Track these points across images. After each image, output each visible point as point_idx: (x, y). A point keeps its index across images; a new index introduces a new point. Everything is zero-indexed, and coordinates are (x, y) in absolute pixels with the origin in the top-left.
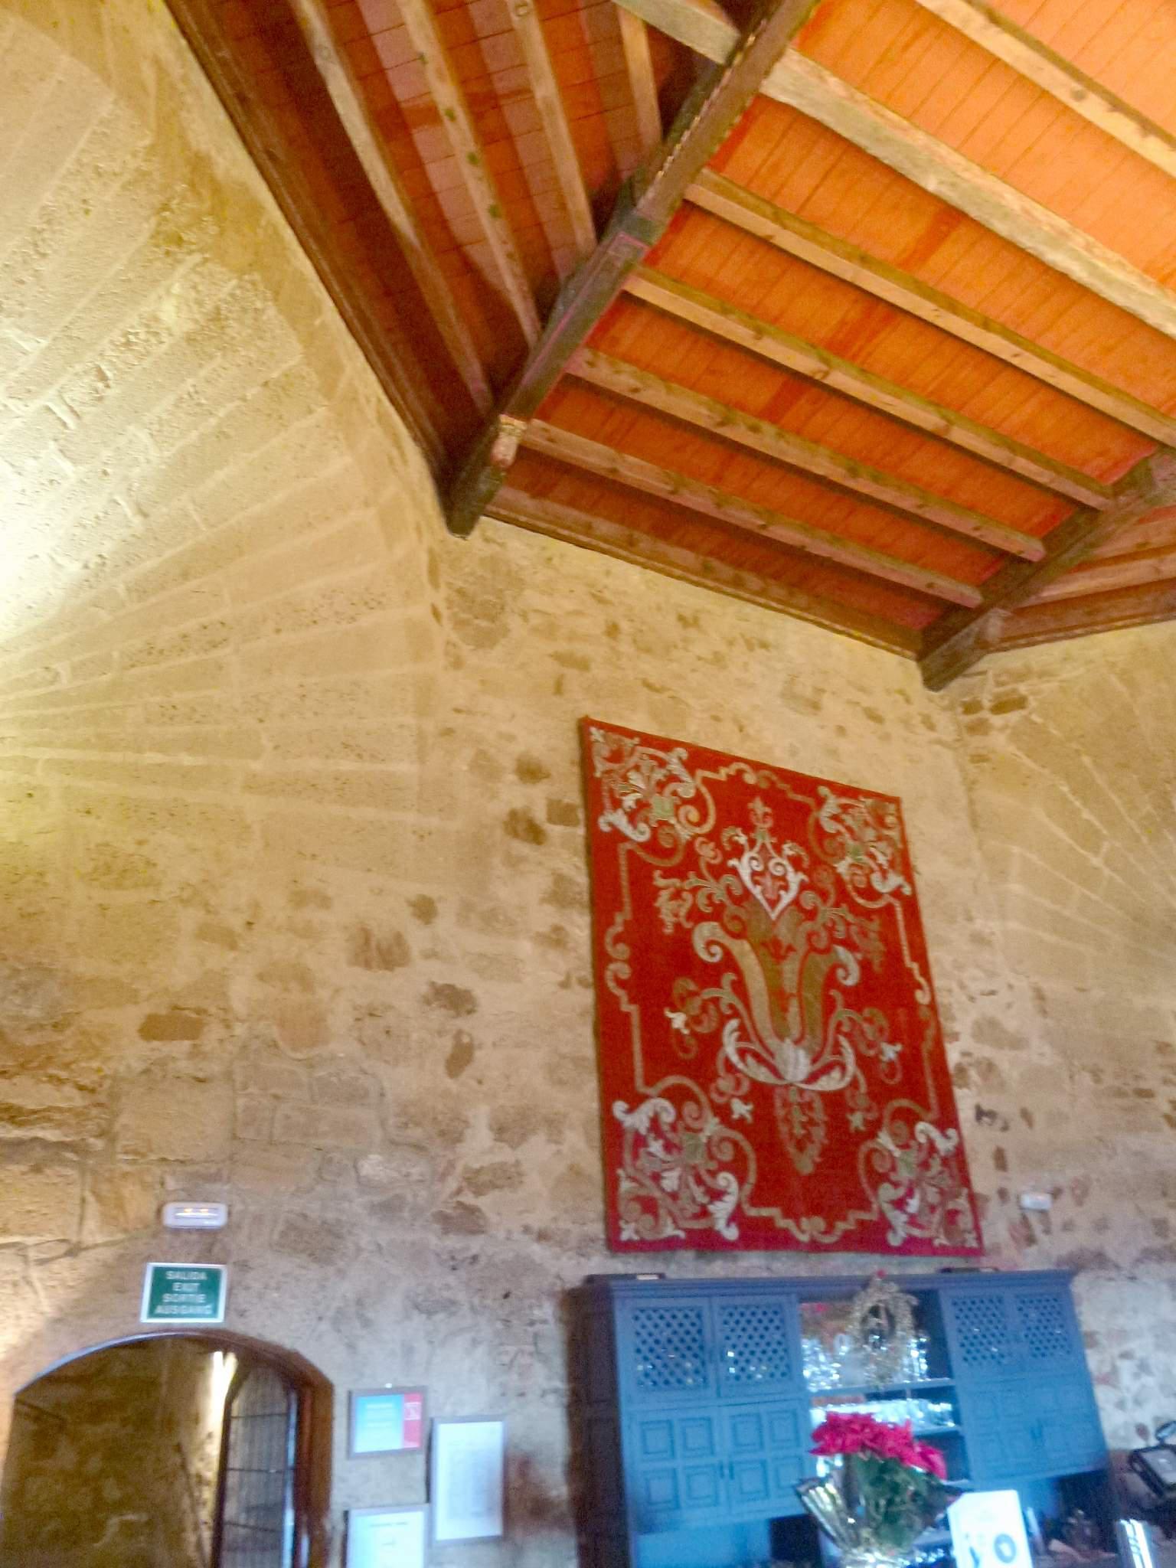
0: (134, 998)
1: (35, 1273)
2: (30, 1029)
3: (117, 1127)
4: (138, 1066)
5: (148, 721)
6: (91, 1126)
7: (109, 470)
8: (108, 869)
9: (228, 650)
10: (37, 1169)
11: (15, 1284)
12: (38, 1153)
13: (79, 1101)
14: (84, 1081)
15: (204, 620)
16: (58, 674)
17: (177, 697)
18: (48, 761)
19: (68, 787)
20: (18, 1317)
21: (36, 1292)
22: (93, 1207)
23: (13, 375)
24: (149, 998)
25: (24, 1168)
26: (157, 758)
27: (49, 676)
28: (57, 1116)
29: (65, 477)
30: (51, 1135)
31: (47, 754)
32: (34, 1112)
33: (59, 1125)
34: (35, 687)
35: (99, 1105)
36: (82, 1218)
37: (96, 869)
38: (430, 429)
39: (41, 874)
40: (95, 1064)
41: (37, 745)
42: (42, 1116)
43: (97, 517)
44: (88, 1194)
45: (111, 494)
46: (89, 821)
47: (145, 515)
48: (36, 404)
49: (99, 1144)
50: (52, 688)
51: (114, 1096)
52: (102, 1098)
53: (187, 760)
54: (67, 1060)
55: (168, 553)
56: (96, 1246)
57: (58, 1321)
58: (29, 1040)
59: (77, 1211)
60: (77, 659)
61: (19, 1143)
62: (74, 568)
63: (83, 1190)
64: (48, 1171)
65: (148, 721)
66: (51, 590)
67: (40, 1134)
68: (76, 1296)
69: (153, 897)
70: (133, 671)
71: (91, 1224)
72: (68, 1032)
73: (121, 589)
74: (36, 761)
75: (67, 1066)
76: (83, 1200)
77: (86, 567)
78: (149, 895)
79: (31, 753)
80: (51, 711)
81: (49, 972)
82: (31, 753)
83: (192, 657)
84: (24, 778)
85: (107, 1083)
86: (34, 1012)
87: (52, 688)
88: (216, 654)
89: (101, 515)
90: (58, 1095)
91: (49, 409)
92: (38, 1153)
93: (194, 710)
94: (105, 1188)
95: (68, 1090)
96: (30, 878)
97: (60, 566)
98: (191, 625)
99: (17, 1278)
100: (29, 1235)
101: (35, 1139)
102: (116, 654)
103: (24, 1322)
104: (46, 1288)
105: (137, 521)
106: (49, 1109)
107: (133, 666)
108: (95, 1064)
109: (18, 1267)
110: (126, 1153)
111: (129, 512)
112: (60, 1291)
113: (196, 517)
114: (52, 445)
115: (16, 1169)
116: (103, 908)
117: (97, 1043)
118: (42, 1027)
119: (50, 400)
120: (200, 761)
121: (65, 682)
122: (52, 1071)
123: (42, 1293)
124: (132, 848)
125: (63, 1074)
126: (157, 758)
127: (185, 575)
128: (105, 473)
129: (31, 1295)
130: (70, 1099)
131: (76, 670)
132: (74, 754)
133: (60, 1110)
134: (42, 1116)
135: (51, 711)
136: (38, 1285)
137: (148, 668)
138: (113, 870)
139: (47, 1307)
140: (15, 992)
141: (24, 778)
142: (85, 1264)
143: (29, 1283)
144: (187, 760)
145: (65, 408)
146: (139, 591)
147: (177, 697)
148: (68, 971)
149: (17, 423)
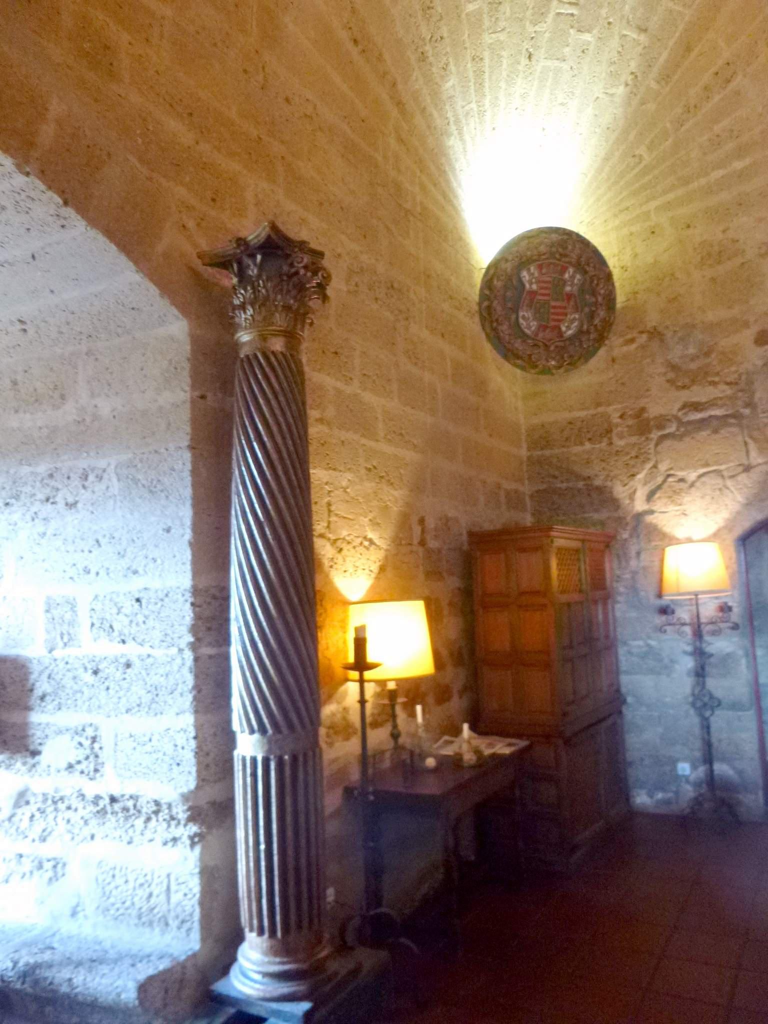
0: (746, 325)
1: (729, 483)
2: (692, 360)
3: (756, 400)
4: (760, 363)
5: (705, 154)
6: (740, 403)
7: (611, 20)
8: (709, 255)
9: (739, 77)
10: (716, 431)
11: (720, 490)
12: (715, 423)
13: (729, 391)
14: (728, 380)
15: (714, 70)
16: (641, 156)
17: (717, 129)
18: (656, 208)
19: (672, 217)
20: (726, 505)
21: (732, 492)
22: (752, 445)
23: (529, 13)
24: (756, 321)
25: (708, 432)
26: (721, 172)
27: (637, 160)
28: (720, 402)
29: (589, 43)
30: (718, 412)
31: (653, 204)
32: (706, 403)
33: (721, 407)
34: (633, 169)
35: (741, 391)
36: (747, 452)
37: (702, 259)
38: (432, 167)
39: (672, 275)
40: (733, 369)
41: (647, 202)
42: (712, 404)
43: (619, 52)
44: (747, 439)
45: (619, 33)
46: (690, 232)
47: (645, 30)
48: (551, 15)
49: (747, 411)
50: (642, 165)
51: (750, 383)
52: (742, 385)
53: (738, 165)
54: (716, 371)
55: (671, 43)
56: (760, 464)
57: (747, 504)
58: (693, 366)
59: (744, 449)
60: (647, 141)
61: (703, 420)
62: (621, 90)
63: (744, 437)
64: (722, 431)
65: (705, 154)
66: (615, 111)
67: (713, 413)
68: (755, 491)
69: (742, 261)
70: (683, 129)
71: (753, 453)
72: (713, 356)
73: (654, 85)
74: (649, 212)
75: (718, 374)
76: (746, 444)
77: (627, 85)
78: (739, 260)
79: (645, 208)
80: (647, 178)
81: (694, 326)
82: (645, 208)
83: (717, 98)
84: (648, 223)
85: (744, 377)
86: (692, 351)
87: (642, 165)
88: (732, 86)
89: (620, 49)
90: (716, 391)
91: (558, 14)
92: (715, 423)
93: (732, 131)
94: (756, 434)
95: (723, 387)
96: (667, 279)
97: (612, 95)
98: (707, 78)
99: (720, 486)
100: (721, 464)
101: (711, 417)
102: (668, 125)
103: (179, 466)
104: (736, 489)
105: (642, 38)
106: (715, 399)
107: (682, 126)
108: (733, 369)
109: (719, 481)
110: (764, 413)
111: (635, 36)
112: (745, 490)
113: (677, 8)
114: (572, 31)
115: (704, 434)
116: (713, 279)
117: (731, 356)
118: (698, 357)
119: (557, 8)
120: (747, 161)
121: (647, 159)
122: (709, 379)
123: (735, 492)
124: (720, 236)
125: (717, 379)
126: (721, 172)
127: (689, 49)
128: (609, 23)
129: (730, 494)
130: (724, 391)
131: (650, 148)
132: (671, 196)
133: (721, 398)
134: (712, 404)
135: (647, 178)
136: (732, 489)
137: (691, 122)
138: (713, 255)
139: (740, 498)
140: (678, 343)
141: (648, 223)
142: (755, 475)
143: (728, 488)
144: (738, 165)
145: (567, 6)
146: (665, 78)
147: (717, 129)
148: (703, 323)
149: (547, 35)
